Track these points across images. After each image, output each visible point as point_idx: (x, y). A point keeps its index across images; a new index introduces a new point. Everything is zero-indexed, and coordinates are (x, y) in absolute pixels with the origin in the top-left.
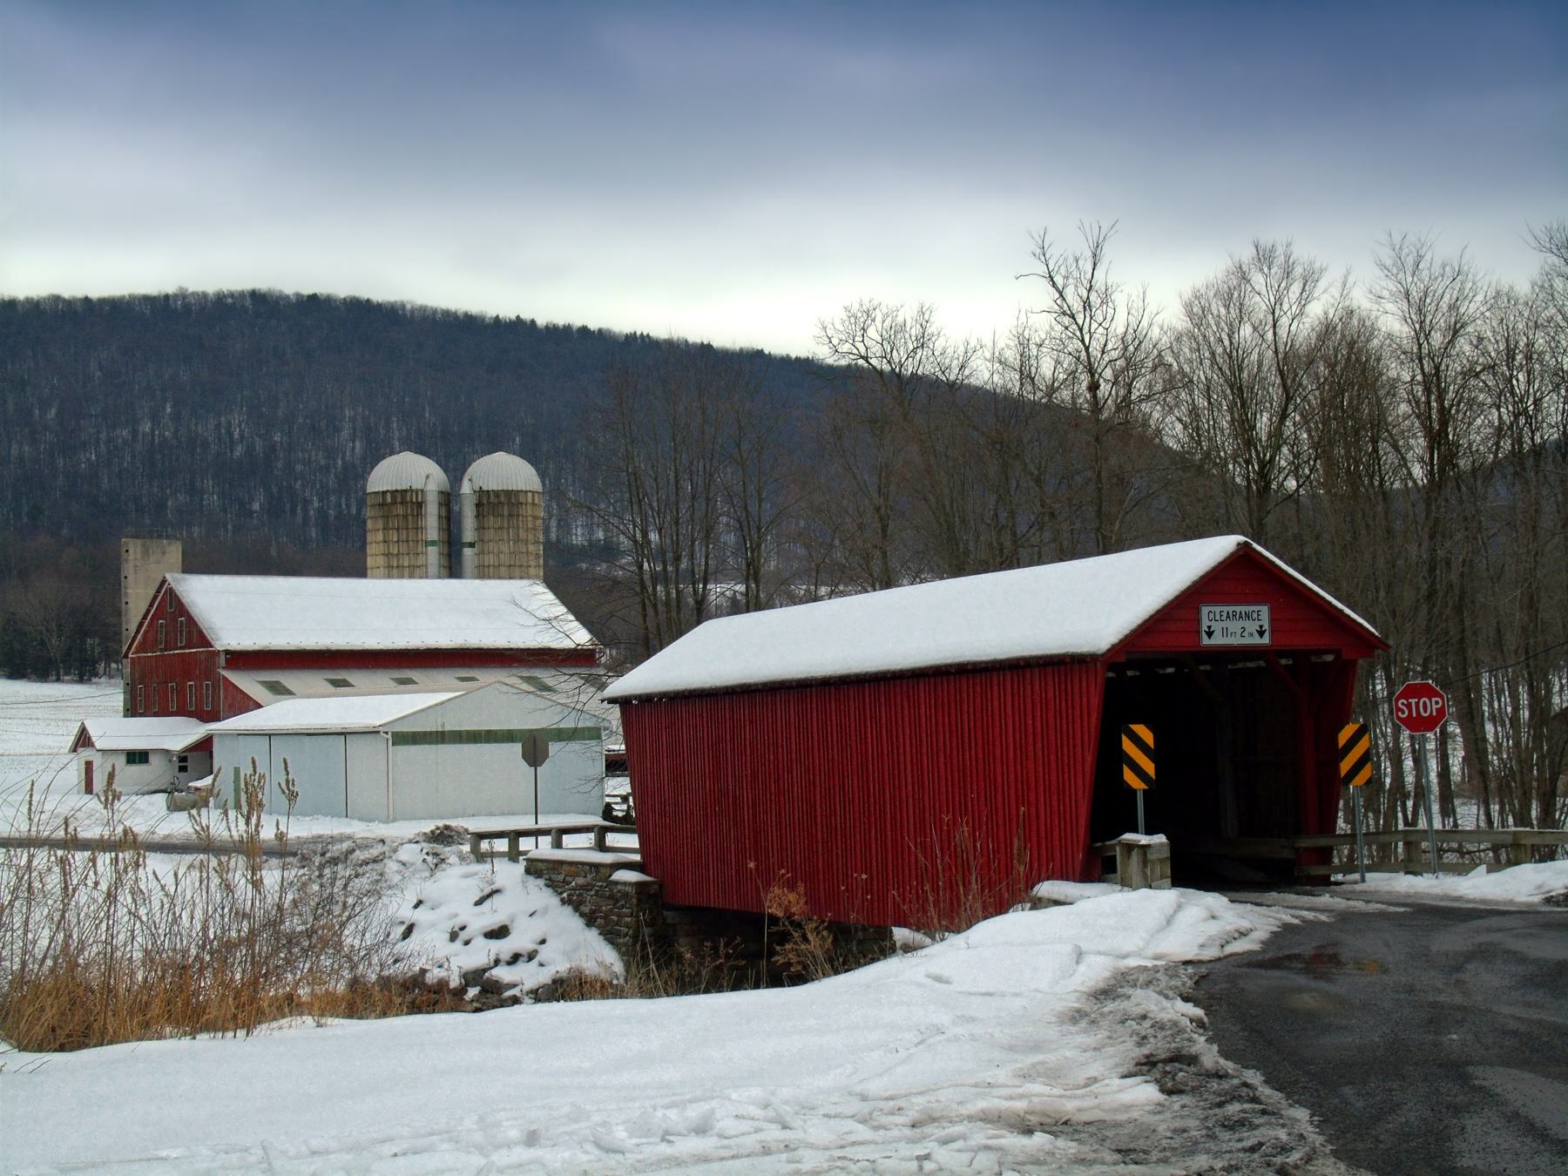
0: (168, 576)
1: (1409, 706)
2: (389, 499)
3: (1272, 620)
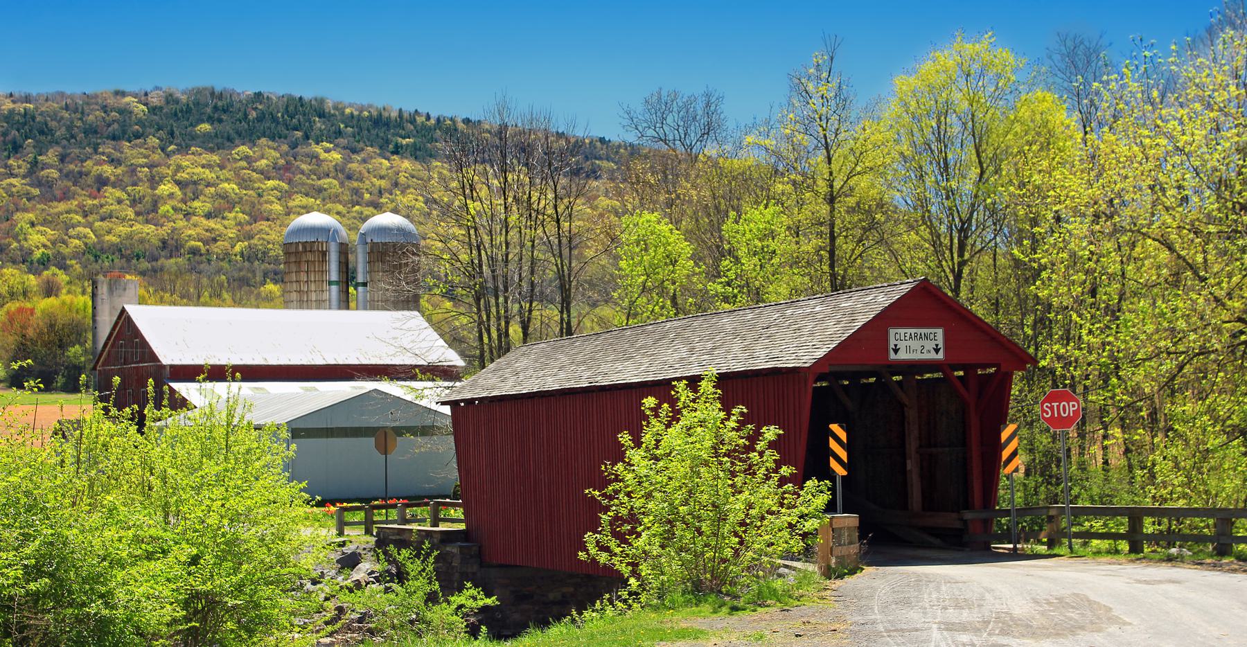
0: (128, 307)
1: (1052, 408)
2: (301, 248)
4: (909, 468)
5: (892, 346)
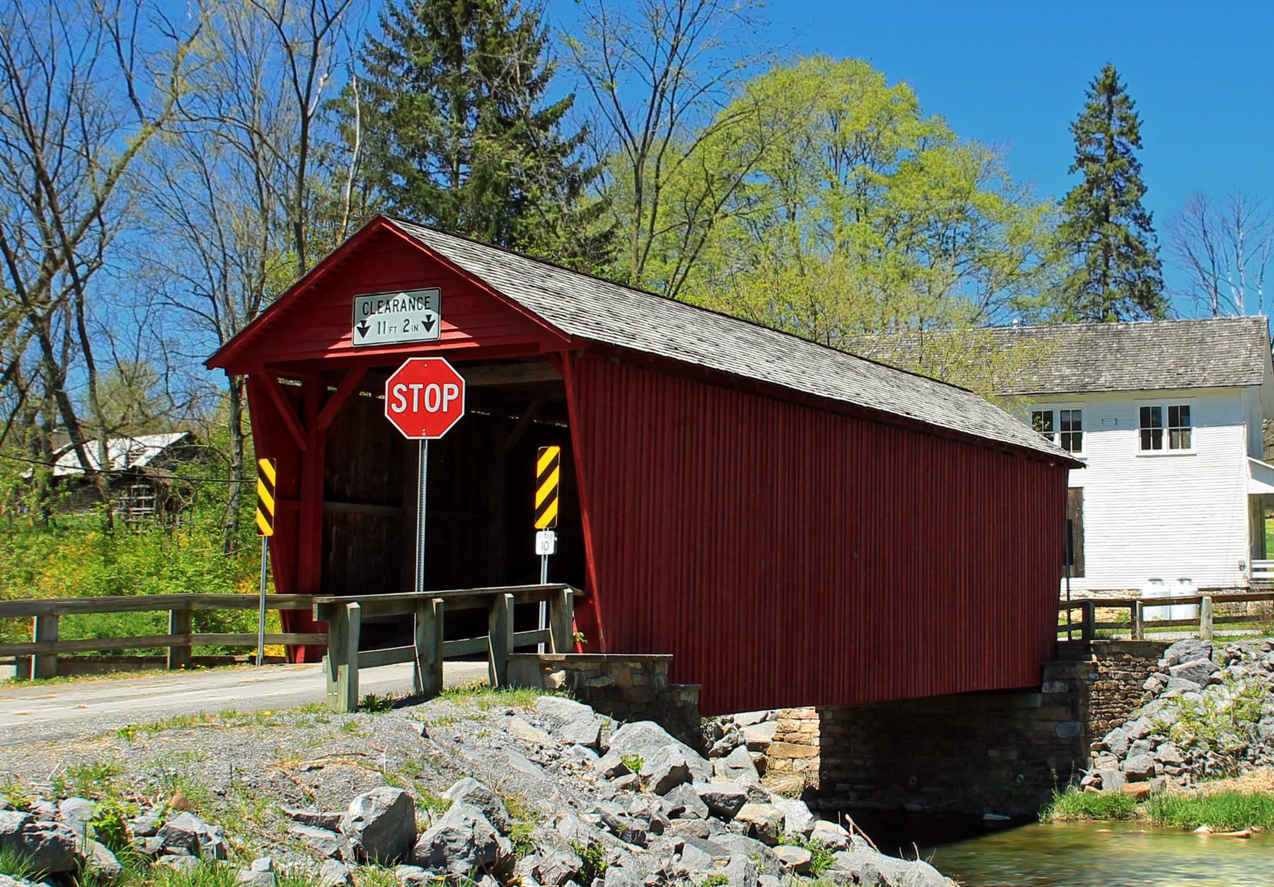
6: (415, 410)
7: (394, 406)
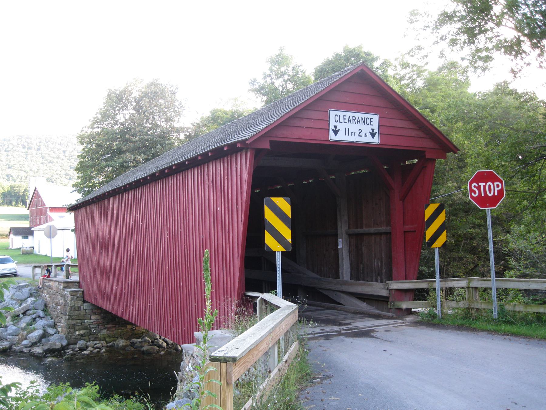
1: (479, 188)
3: (381, 126)
4: (340, 246)
5: (332, 127)
6: (483, 195)
7: (473, 193)
